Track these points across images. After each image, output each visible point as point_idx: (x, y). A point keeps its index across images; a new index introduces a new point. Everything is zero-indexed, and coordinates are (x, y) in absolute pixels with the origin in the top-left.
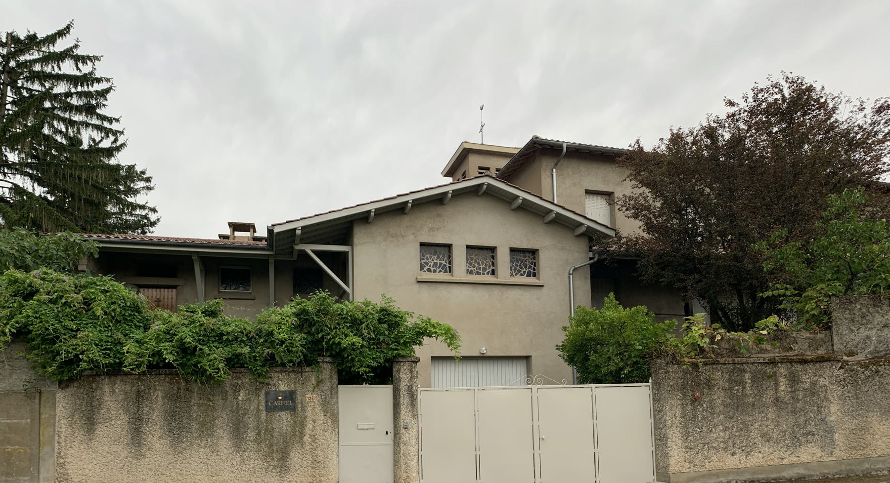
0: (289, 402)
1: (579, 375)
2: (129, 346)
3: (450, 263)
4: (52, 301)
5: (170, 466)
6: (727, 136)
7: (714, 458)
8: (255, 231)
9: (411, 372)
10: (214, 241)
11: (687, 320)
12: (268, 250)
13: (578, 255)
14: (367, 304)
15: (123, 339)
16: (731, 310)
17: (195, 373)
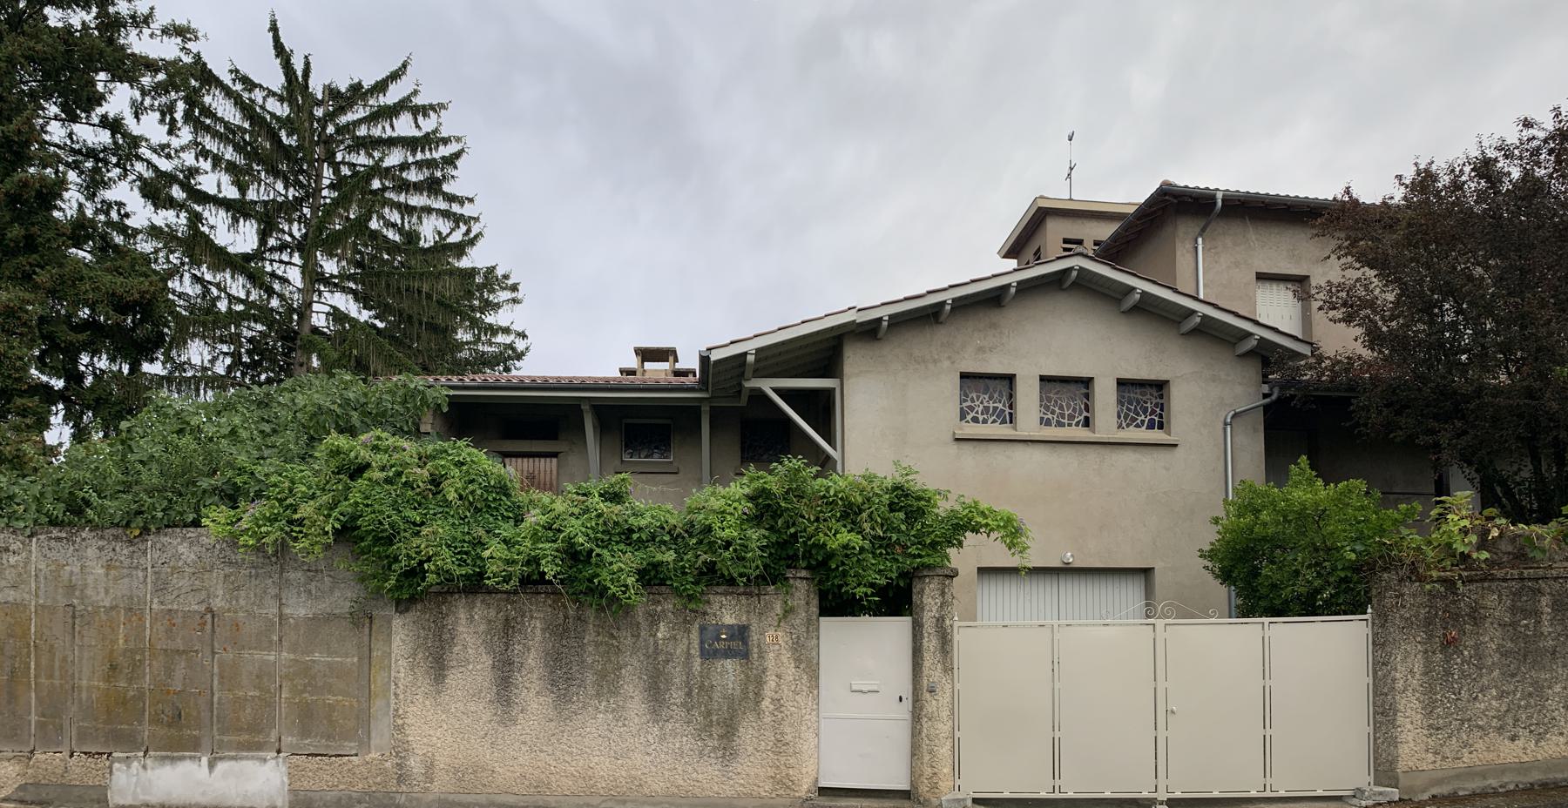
0: (739, 643)
1: (1240, 602)
2: (494, 549)
3: (1011, 407)
4: (388, 481)
5: (553, 740)
6: (1516, 174)
7: (1480, 745)
8: (676, 360)
9: (943, 594)
10: (614, 379)
11: (1438, 502)
12: (700, 390)
13: (1240, 390)
14: (870, 478)
15: (485, 539)
16: (1518, 484)
17: (590, 591)
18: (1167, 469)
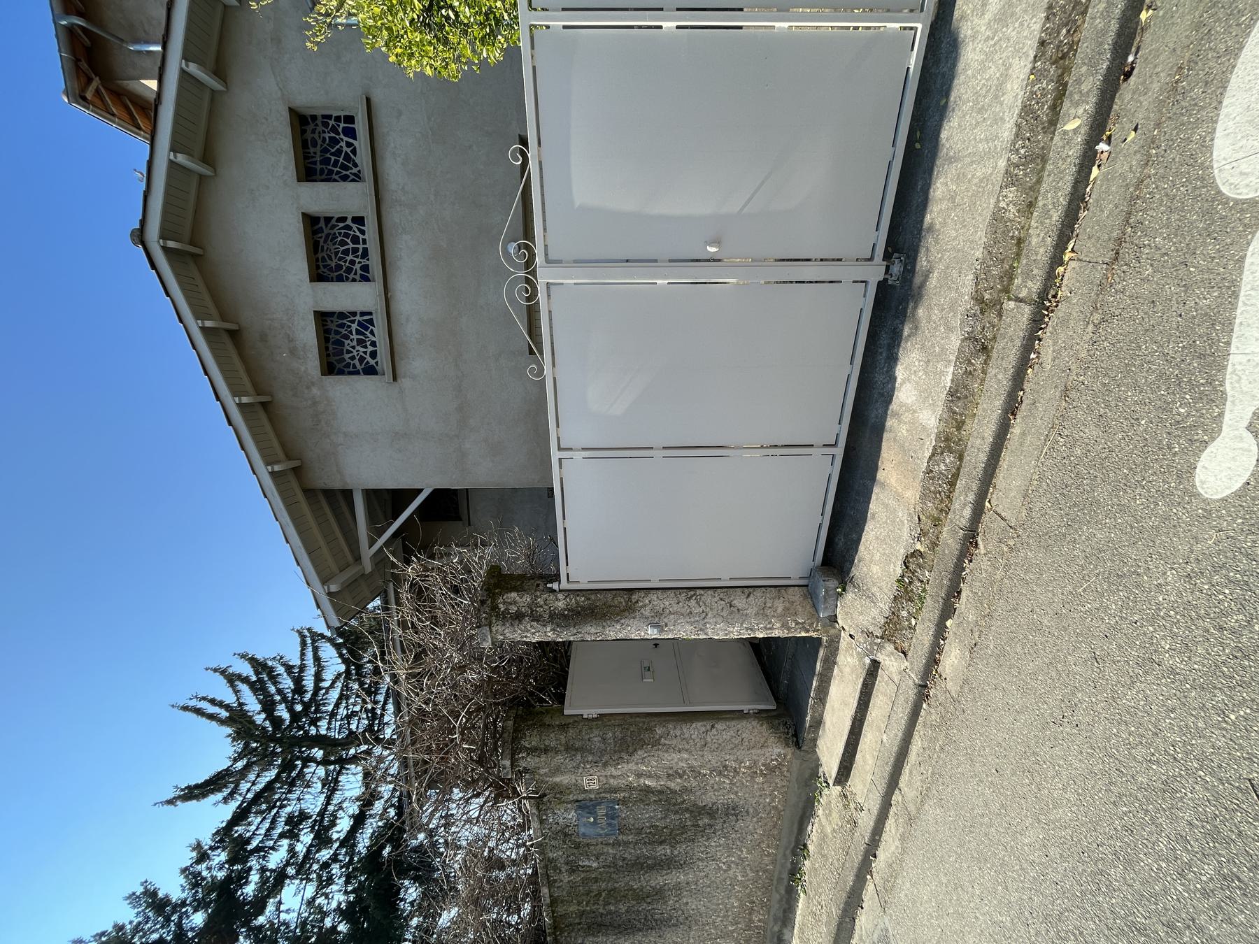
18: (400, 113)
